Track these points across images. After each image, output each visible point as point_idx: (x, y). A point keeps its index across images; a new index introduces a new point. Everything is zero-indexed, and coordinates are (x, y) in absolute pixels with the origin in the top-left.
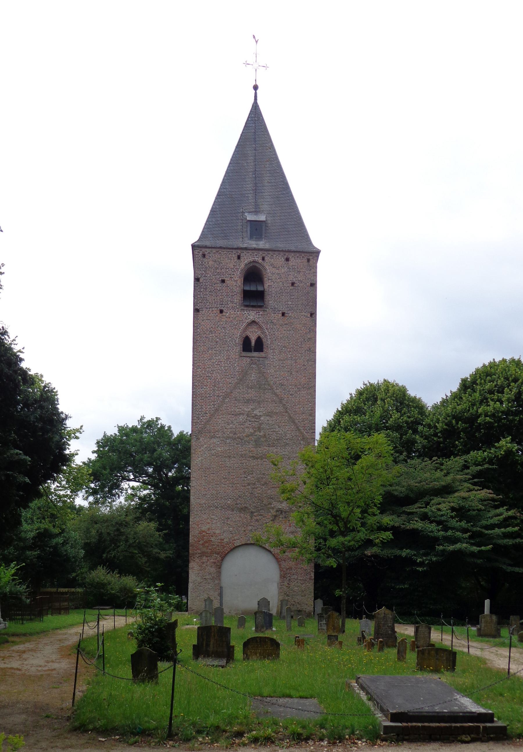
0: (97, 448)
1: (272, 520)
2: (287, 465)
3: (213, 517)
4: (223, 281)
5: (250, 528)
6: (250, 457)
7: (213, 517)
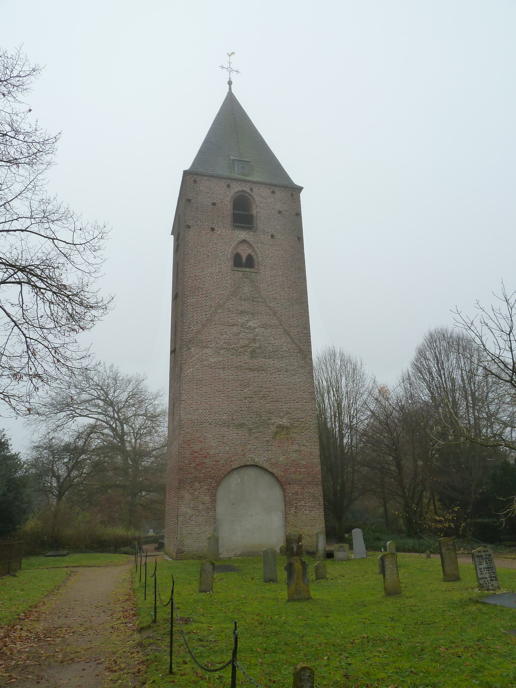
6: (246, 369)
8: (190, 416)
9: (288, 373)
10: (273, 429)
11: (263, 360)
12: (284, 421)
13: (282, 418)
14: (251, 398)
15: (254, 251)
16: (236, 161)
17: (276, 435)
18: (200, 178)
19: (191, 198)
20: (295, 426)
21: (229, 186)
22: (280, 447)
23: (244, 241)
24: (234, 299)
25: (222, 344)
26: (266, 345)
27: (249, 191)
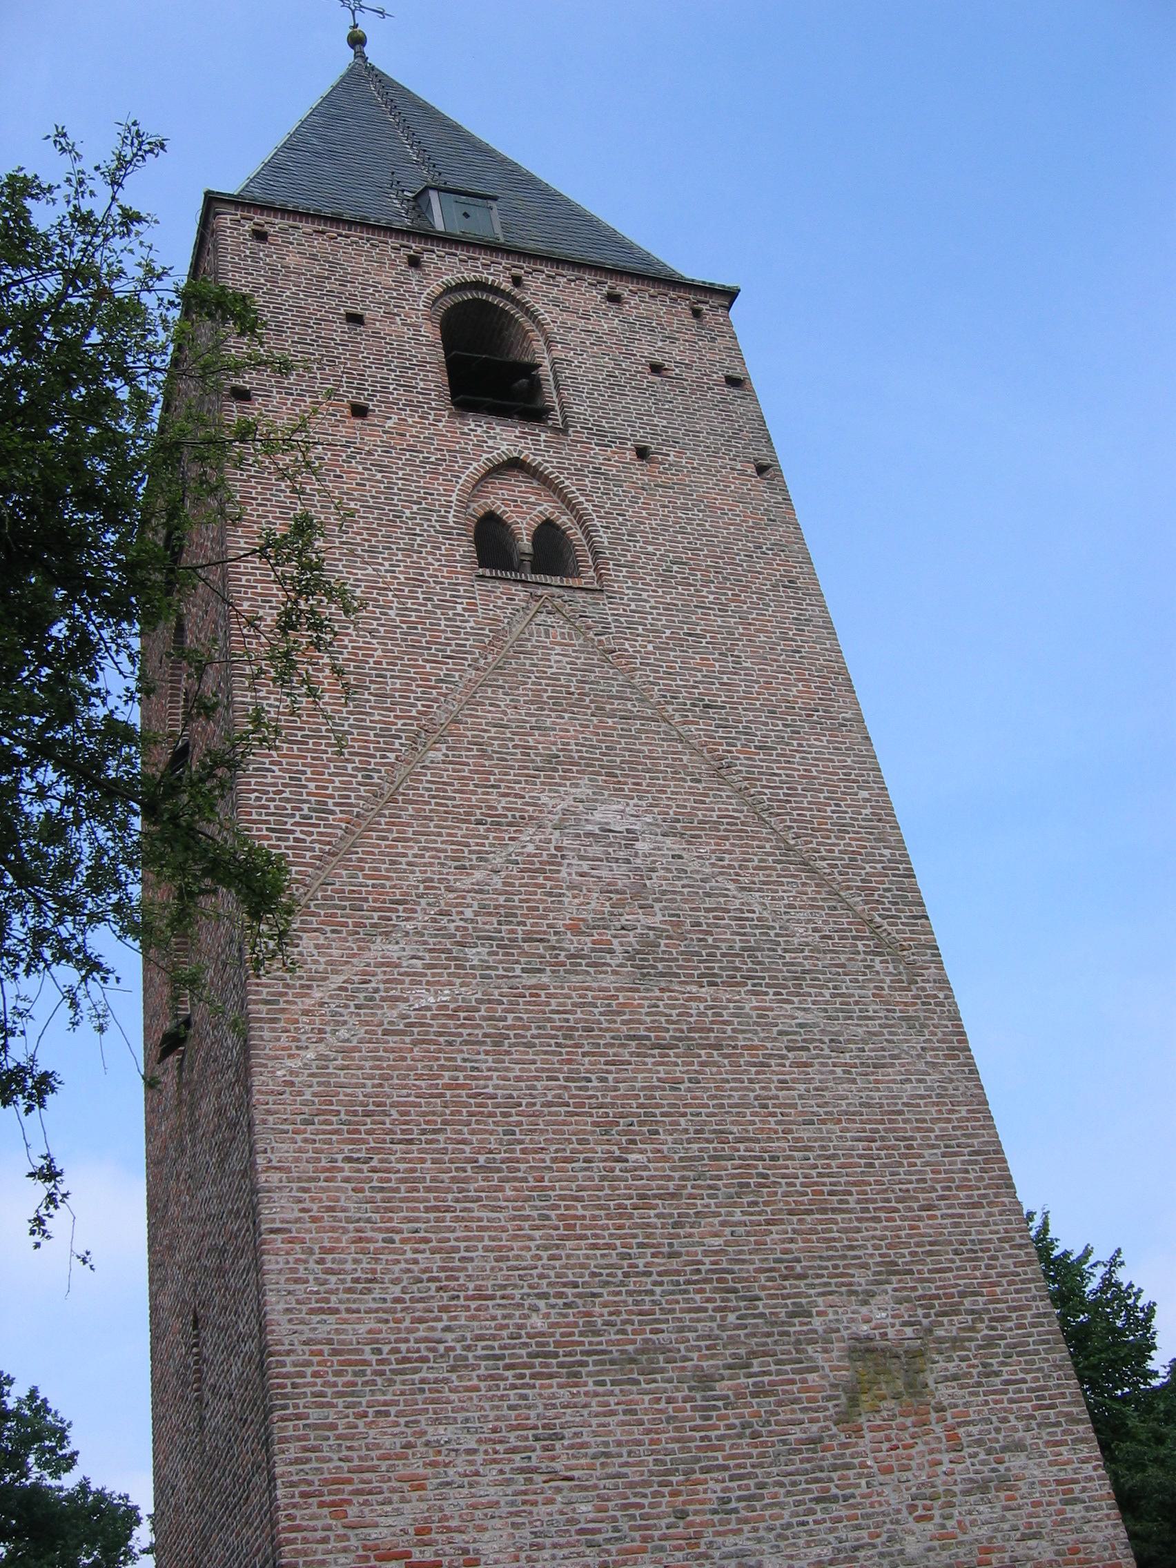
0: (93, 1489)
1: (842, 1419)
2: (838, 1081)
3: (442, 1433)
4: (355, 319)
5: (713, 1488)
6: (623, 1040)
7: (442, 1433)
8: (325, 1327)
9: (846, 1058)
10: (831, 1366)
11: (706, 991)
12: (881, 1317)
13: (867, 1298)
14: (673, 1196)
15: (571, 506)
16: (433, 195)
17: (854, 1402)
18: (280, 222)
19: (246, 291)
20: (940, 1340)
21: (414, 262)
22: (888, 1470)
23: (515, 465)
24: (504, 701)
25: (469, 913)
26: (706, 919)
27: (507, 286)
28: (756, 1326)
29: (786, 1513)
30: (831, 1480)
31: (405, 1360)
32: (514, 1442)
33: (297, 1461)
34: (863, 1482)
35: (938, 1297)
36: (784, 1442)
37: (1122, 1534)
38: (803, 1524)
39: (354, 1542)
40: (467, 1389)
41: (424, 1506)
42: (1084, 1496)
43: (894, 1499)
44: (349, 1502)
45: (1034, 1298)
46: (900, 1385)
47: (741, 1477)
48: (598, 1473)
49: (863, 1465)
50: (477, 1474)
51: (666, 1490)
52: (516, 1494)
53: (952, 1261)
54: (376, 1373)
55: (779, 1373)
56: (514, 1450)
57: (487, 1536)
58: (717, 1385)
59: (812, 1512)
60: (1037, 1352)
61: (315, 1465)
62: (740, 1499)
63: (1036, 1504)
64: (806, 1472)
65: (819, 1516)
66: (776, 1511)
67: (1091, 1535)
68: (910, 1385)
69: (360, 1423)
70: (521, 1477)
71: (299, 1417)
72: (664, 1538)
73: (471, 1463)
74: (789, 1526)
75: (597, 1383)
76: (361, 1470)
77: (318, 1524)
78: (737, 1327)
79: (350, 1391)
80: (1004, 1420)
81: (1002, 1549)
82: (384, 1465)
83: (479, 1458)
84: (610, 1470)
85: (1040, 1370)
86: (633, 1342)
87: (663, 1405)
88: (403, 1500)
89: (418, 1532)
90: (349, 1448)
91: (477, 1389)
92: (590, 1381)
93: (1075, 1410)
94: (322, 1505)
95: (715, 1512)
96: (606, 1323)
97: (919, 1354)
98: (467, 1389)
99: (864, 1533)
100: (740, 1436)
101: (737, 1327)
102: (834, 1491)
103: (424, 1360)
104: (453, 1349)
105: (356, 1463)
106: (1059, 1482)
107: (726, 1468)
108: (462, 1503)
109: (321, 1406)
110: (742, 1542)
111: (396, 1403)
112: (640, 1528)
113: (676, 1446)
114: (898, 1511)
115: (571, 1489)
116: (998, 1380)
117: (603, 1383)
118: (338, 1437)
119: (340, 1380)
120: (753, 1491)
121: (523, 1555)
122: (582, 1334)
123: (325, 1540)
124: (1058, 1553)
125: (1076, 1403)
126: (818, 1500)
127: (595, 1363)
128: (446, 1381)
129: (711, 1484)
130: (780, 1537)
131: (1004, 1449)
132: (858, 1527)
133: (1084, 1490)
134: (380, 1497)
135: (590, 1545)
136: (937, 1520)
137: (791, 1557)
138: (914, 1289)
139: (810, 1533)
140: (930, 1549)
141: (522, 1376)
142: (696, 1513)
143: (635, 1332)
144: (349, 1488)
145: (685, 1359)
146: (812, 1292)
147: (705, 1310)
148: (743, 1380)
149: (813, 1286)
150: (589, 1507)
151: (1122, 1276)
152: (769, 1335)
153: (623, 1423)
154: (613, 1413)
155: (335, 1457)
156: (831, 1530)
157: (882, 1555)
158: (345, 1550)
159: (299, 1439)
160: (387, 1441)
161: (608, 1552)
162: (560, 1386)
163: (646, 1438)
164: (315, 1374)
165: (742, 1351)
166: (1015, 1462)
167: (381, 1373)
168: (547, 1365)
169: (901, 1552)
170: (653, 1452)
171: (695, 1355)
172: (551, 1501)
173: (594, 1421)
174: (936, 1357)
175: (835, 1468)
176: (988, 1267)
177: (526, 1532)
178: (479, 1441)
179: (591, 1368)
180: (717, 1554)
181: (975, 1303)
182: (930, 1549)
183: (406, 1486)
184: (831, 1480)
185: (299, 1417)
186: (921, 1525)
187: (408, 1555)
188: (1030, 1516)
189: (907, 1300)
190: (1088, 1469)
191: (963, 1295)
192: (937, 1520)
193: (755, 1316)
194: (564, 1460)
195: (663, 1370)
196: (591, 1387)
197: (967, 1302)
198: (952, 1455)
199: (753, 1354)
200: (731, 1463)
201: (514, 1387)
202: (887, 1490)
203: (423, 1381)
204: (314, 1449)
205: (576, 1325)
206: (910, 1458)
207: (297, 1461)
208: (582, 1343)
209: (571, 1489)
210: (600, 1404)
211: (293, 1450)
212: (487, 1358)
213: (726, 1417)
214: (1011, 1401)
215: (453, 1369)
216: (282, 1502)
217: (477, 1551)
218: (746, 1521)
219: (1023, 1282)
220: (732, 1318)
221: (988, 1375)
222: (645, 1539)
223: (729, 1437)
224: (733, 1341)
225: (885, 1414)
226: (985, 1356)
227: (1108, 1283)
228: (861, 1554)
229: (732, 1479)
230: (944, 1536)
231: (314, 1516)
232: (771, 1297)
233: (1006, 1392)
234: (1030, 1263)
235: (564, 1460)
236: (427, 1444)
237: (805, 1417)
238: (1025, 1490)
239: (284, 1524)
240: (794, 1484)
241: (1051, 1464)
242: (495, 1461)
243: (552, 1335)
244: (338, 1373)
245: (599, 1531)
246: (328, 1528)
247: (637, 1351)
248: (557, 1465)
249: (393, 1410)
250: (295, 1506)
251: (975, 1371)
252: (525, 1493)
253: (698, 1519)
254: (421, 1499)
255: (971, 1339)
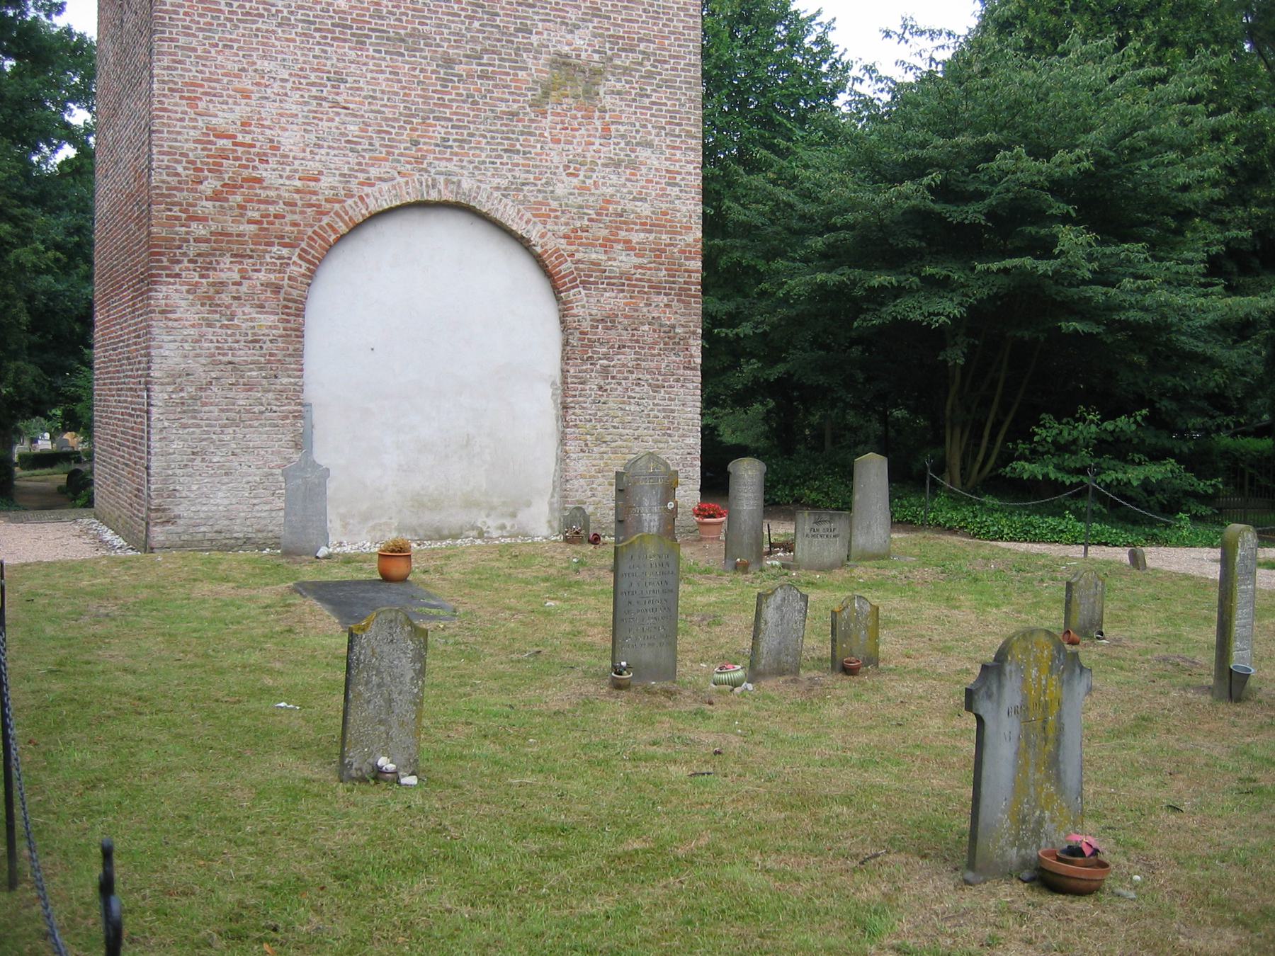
3: (266, 65)
5: (439, 131)
7: (266, 65)
10: (536, 68)
12: (581, 44)
13: (573, 28)
17: (546, 95)
20: (616, 67)
22: (558, 141)
28: (492, 33)
29: (484, 155)
30: (518, 140)
31: (248, 14)
32: (313, 79)
33: (168, 68)
34: (539, 146)
35: (623, 38)
36: (493, 111)
37: (699, 209)
38: (493, 163)
39: (200, 124)
40: (287, 40)
41: (249, 109)
42: (682, 183)
43: (556, 159)
44: (200, 99)
45: (690, 53)
46: (580, 90)
47: (459, 127)
48: (366, 107)
49: (541, 135)
50: (286, 95)
51: (408, 127)
52: (309, 111)
53: (641, 16)
54: (226, 19)
55: (500, 66)
56: (313, 84)
57: (287, 134)
58: (457, 67)
59: (500, 157)
60: (680, 88)
61: (180, 72)
62: (455, 140)
63: (649, 181)
64: (503, 132)
65: (505, 160)
66: (478, 152)
67: (678, 207)
68: (586, 92)
69: (213, 51)
70: (314, 102)
71: (172, 40)
72: (401, 155)
73: (283, 87)
74: (484, 162)
75: (375, 51)
76: (210, 80)
77: (179, 109)
78: (478, 31)
79: (208, 28)
80: (645, 126)
81: (618, 203)
82: (225, 80)
83: (289, 85)
84: (373, 108)
85: (679, 100)
86: (405, 28)
87: (417, 73)
88: (235, 103)
89: (243, 124)
90: (204, 65)
91: (294, 41)
92: (371, 49)
93: (693, 130)
94: (182, 98)
95: (437, 145)
96: (390, 13)
97: (599, 73)
98: (287, 40)
99: (532, 176)
100: (464, 102)
101: (478, 31)
102: (518, 147)
103: (262, 16)
104: (281, 12)
105: (208, 75)
106: (667, 171)
107: (451, 120)
108: (274, 112)
109: (188, 35)
110: (451, 167)
111: (239, 41)
112: (387, 146)
113: (421, 100)
114: (557, 167)
115: (346, 115)
116: (647, 101)
117: (380, 52)
118: (197, 57)
119: (202, 20)
120: (465, 137)
121: (308, 150)
122: (371, 16)
123: (182, 120)
124: (653, 213)
125: (697, 126)
126: (506, 151)
127: (377, 38)
128: (274, 32)
129: (439, 128)
130: (476, 167)
131: (638, 144)
132: (528, 172)
133: (683, 179)
134: (221, 99)
135: (352, 150)
136: (581, 177)
137: (480, 181)
138: (608, 29)
139: (496, 169)
140: (571, 194)
141: (326, 38)
142: (425, 144)
143: (407, 22)
144: (201, 90)
145: (439, 46)
146: (536, 17)
147: (459, 16)
148: (474, 66)
149: (537, 13)
150: (356, 128)
151: (832, 37)
152: (499, 40)
153: (388, 80)
154: (382, 72)
155: (194, 69)
156: (510, 170)
157: (539, 191)
158: (194, 128)
159: (170, 54)
160: (229, 65)
161: (364, 157)
162: (350, 48)
163: (402, 93)
164: (186, 14)
165: (479, 48)
166: (643, 153)
167: (231, 20)
168: (344, 33)
169: (552, 192)
170: (404, 101)
171: (446, 45)
172: (332, 120)
173: (369, 75)
174: (610, 77)
175: (522, 133)
176: (664, 25)
177: (313, 136)
178: (290, 75)
179: (373, 40)
180: (433, 171)
181: (647, 47)
182: (571, 194)
183: (238, 95)
184: (518, 140)
185: (172, 40)
186: (570, 179)
187: (235, 137)
188: (642, 187)
189: (601, 36)
190: (690, 168)
191: (640, 40)
192: (581, 177)
193: (492, 26)
194: (344, 96)
195: (422, 50)
196: (371, 53)
197: (642, 46)
198: (602, 141)
199: (485, 51)
200: (455, 118)
201: (319, 43)
202: (553, 153)
203: (258, 30)
204: (180, 62)
205: (368, 10)
206: (574, 137)
207: (168, 68)
208: (370, 23)
209: (346, 115)
210: (375, 65)
211: (166, 61)
212: (304, 21)
213: (458, 88)
214: (652, 115)
215: (279, 25)
216: (156, 92)
217: (279, 142)
218: (457, 154)
219: (685, 40)
220: (476, 24)
221: (642, 96)
222: (388, 153)
223: (457, 101)
224: (474, 40)
225: (565, 106)
226: (644, 83)
227: (820, 41)
228: (526, 188)
229: (453, 127)
230: (583, 188)
231: (176, 103)
232: (507, 15)
233: (651, 109)
234: (694, 29)
235: (344, 96)
236: (256, 71)
237: (511, 98)
238: (644, 171)
239: (156, 105)
240: (493, 138)
241: (666, 159)
242: (299, 89)
243: (351, 14)
244: (201, 15)
245: (360, 143)
246: (186, 113)
247: (406, 34)
248: (339, 99)
249: (236, 45)
250: (164, 96)
251: (633, 92)
252: (315, 112)
253: (425, 148)
254: (247, 105)
255: (637, 71)
